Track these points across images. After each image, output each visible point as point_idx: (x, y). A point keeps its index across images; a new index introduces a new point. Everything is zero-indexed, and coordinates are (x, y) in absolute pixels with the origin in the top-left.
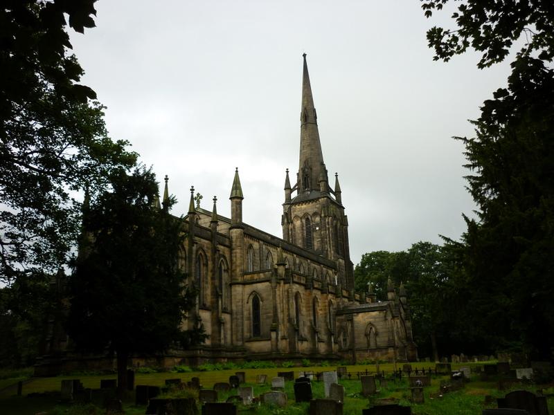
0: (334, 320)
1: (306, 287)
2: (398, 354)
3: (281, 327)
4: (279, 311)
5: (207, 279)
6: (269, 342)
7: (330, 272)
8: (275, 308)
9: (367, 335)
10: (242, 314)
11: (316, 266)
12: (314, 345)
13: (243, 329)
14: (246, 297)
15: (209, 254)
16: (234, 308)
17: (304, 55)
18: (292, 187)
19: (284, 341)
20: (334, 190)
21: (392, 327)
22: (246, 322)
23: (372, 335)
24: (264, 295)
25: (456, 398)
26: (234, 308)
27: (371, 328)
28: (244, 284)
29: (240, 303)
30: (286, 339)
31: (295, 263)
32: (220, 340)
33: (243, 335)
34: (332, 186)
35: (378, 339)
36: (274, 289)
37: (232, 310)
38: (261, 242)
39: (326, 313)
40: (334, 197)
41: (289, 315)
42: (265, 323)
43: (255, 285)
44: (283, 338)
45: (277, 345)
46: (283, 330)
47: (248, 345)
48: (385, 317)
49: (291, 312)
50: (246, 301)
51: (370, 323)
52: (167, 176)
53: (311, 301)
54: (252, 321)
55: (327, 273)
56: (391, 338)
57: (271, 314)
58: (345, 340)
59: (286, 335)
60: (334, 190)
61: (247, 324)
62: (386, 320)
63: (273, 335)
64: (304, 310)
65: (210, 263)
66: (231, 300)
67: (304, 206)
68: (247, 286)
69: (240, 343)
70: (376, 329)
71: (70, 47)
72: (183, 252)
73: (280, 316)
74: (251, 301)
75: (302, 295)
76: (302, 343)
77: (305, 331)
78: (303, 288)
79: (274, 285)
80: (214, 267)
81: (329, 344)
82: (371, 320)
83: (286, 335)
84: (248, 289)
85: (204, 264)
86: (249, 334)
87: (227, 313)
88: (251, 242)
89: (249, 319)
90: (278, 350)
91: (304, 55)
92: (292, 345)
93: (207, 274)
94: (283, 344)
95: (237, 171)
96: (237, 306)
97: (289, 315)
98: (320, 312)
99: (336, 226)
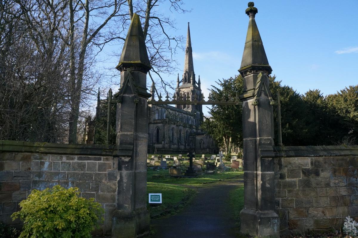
0: (189, 137)
1: (184, 127)
2: (210, 151)
3: (166, 140)
4: (165, 134)
6: (162, 145)
7: (192, 117)
8: (164, 133)
9: (200, 143)
10: (153, 134)
11: (185, 115)
12: (179, 146)
13: (153, 140)
14: (154, 128)
16: (150, 132)
17: (189, 23)
18: (180, 81)
19: (167, 145)
21: (209, 141)
22: (154, 137)
23: (202, 144)
24: (161, 128)
25: (32, 163)
28: (154, 123)
29: (152, 131)
30: (167, 144)
33: (153, 142)
34: (197, 80)
35: (204, 145)
36: (164, 126)
40: (197, 85)
41: (169, 136)
42: (161, 137)
43: (157, 124)
44: (167, 143)
45: (164, 146)
46: (167, 140)
48: (207, 137)
49: (170, 135)
50: (154, 130)
51: (201, 139)
53: (179, 131)
54: (156, 137)
55: (191, 118)
56: (208, 145)
57: (163, 135)
58: (192, 145)
59: (168, 143)
61: (154, 139)
62: (207, 138)
63: (163, 142)
64: (175, 134)
68: (155, 124)
69: (151, 145)
70: (203, 141)
71: (110, 91)
73: (166, 136)
75: (175, 129)
76: (174, 146)
77: (175, 141)
78: (183, 127)
79: (164, 125)
81: (185, 146)
82: (202, 138)
83: (168, 143)
84: (155, 125)
89: (155, 136)
90: (279, 84)
91: (189, 23)
92: (170, 146)
94: (167, 146)
96: (151, 132)
97: (169, 136)
98: (183, 134)
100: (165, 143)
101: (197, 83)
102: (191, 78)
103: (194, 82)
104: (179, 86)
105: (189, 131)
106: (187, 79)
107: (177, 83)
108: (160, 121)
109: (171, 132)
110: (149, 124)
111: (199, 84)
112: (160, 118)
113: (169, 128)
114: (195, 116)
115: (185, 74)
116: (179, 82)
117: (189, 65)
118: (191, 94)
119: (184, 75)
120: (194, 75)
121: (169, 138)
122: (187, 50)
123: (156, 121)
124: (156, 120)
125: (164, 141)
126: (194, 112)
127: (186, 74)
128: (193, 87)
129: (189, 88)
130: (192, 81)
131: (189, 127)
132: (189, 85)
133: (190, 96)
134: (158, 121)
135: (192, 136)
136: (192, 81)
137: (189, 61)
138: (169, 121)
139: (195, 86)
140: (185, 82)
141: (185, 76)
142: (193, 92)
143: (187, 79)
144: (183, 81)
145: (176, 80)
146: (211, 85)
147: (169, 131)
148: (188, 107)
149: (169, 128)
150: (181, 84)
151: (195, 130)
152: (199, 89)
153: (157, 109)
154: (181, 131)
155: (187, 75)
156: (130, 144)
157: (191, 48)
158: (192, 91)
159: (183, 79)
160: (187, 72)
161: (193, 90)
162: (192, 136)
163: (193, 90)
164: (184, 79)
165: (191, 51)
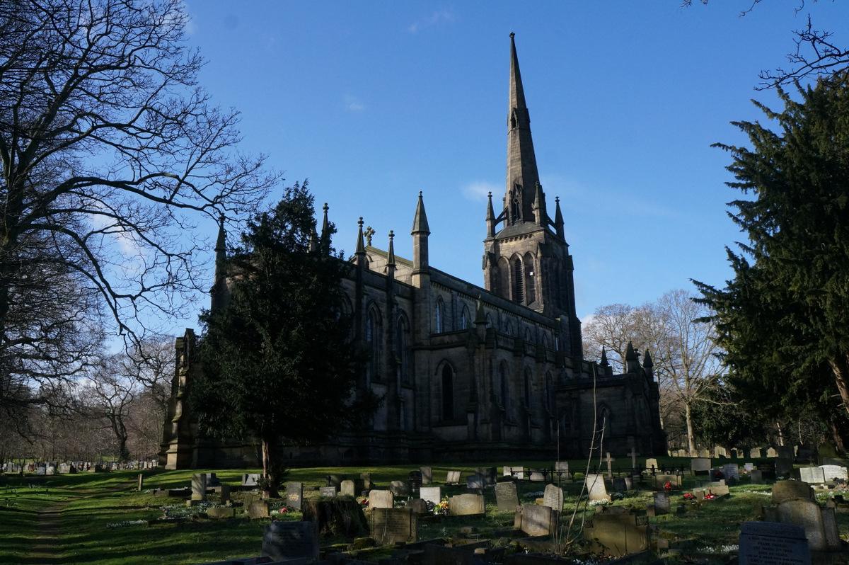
5: (381, 342)
6: (465, 428)
7: (549, 333)
11: (530, 325)
14: (434, 366)
15: (384, 309)
17: (513, 35)
19: (485, 427)
20: (554, 221)
22: (434, 401)
26: (418, 382)
27: (604, 410)
28: (432, 348)
29: (426, 376)
30: (488, 423)
31: (499, 321)
32: (399, 425)
34: (552, 215)
37: (414, 385)
38: (454, 293)
39: (542, 390)
40: (554, 231)
44: (484, 422)
47: (437, 431)
52: (326, 204)
60: (554, 221)
63: (471, 418)
64: (511, 386)
65: (385, 321)
66: (414, 370)
67: (513, 243)
69: (425, 429)
72: (349, 307)
73: (480, 392)
74: (440, 372)
75: (509, 364)
76: (509, 430)
77: (514, 413)
80: (391, 327)
82: (605, 399)
84: (437, 355)
85: (377, 323)
86: (437, 417)
87: (410, 389)
88: (441, 292)
93: (381, 336)
95: (421, 197)
98: (535, 388)
99: (557, 270)
100: (479, 419)
101: (551, 222)
102: (535, 205)
103: (545, 219)
104: (493, 233)
105: (554, 374)
106: (520, 208)
107: (488, 224)
108: (455, 338)
109: (497, 378)
110: (413, 350)
111: (559, 223)
112: (448, 329)
113: (491, 361)
114: (556, 327)
115: (512, 193)
116: (494, 221)
117: (523, 165)
118: (539, 255)
119: (508, 198)
120: (542, 196)
121: (493, 399)
122: (513, 120)
123: (439, 339)
124: (438, 335)
125: (475, 412)
126: (552, 314)
127: (517, 193)
128: (542, 233)
129: (530, 236)
130: (536, 213)
131: (553, 360)
132: (529, 226)
133: (536, 264)
134: (447, 339)
135: (564, 391)
136: (536, 213)
137: (521, 152)
138: (476, 340)
139: (547, 231)
140: (514, 219)
141: (511, 201)
142: (543, 246)
143: (520, 208)
144: (507, 218)
145: (485, 214)
146: (714, 145)
147: (491, 372)
148: (530, 300)
149: (491, 361)
150: (500, 227)
151: (569, 372)
152: (560, 239)
153: (440, 300)
154: (530, 376)
155: (521, 197)
156: (497, 345)
157: (526, 111)
158: (540, 244)
159: (506, 211)
160: (518, 186)
161: (543, 242)
162: (567, 394)
163: (543, 242)
164: (510, 210)
165: (528, 121)
